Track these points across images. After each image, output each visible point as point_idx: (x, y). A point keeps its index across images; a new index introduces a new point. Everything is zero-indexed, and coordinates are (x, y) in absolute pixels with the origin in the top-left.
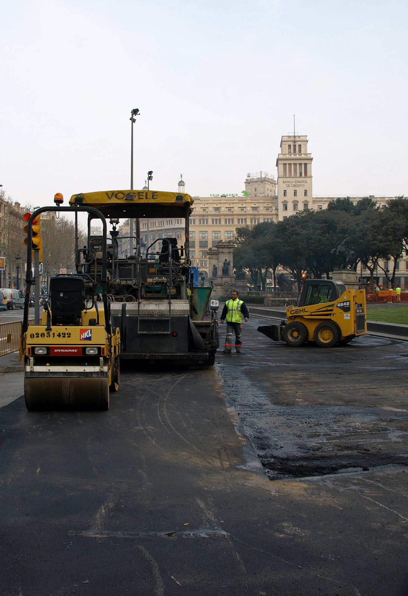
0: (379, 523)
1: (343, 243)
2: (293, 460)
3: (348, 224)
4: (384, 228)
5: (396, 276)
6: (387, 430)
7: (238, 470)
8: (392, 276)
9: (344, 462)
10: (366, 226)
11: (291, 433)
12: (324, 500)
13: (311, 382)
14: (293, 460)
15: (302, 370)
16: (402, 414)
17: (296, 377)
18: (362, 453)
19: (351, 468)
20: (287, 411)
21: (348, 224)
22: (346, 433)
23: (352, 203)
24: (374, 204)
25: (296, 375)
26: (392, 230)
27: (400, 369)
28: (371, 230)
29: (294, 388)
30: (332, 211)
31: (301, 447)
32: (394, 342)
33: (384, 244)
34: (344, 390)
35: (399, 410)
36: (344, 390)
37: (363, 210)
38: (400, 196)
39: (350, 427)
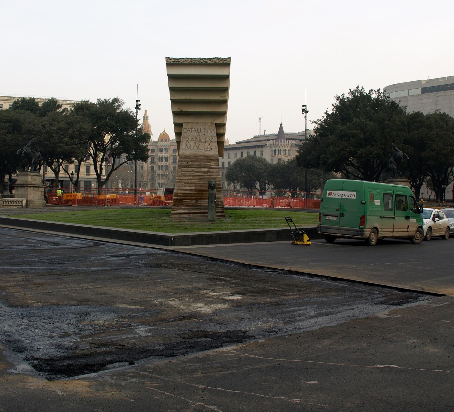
0: (173, 409)
1: (29, 144)
2: (58, 360)
3: (34, 125)
4: (70, 131)
5: (79, 179)
6: (131, 326)
7: (11, 374)
8: (76, 179)
9: (109, 358)
10: (53, 128)
11: (40, 334)
12: (111, 394)
13: (35, 284)
14: (58, 360)
15: (19, 272)
16: (138, 311)
17: (16, 279)
18: (120, 349)
19: (118, 363)
20: (26, 313)
21: (34, 125)
22: (95, 331)
23: (37, 104)
24: (445, 114)
25: (16, 277)
26: (78, 133)
27: (115, 269)
28: (57, 132)
29: (20, 290)
30: (17, 110)
31: (59, 347)
32: (97, 244)
33: (70, 147)
34: (71, 290)
35: (133, 307)
36: (71, 290)
37: (49, 111)
38: (86, 100)
39: (95, 325)
